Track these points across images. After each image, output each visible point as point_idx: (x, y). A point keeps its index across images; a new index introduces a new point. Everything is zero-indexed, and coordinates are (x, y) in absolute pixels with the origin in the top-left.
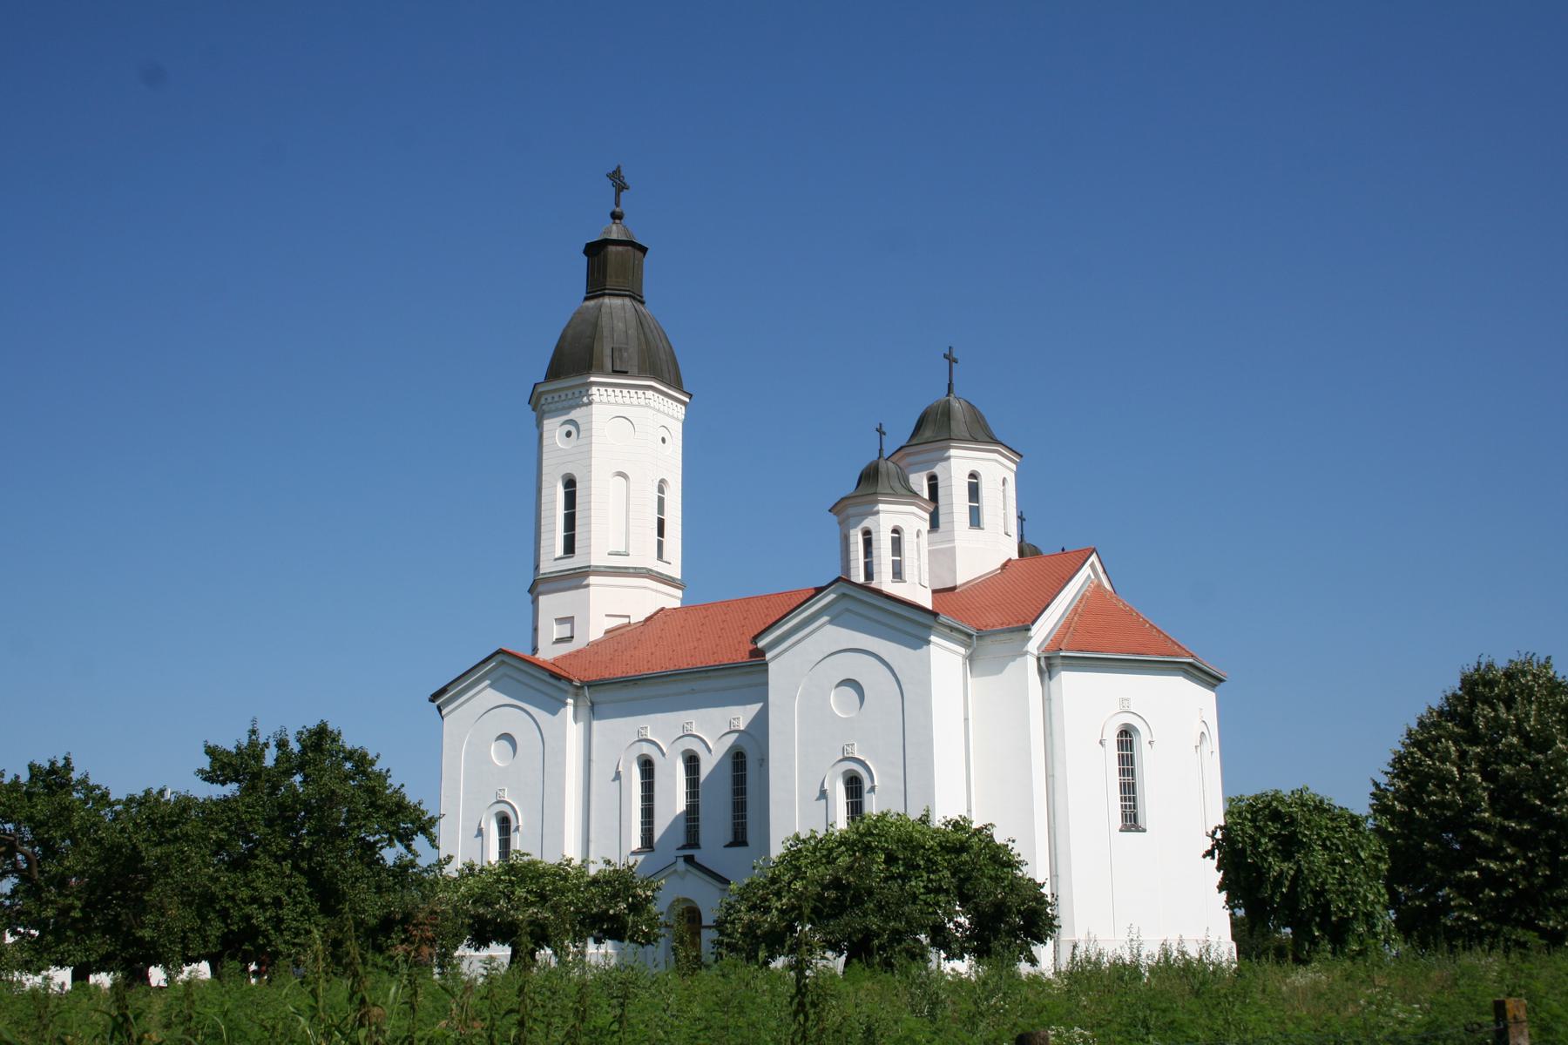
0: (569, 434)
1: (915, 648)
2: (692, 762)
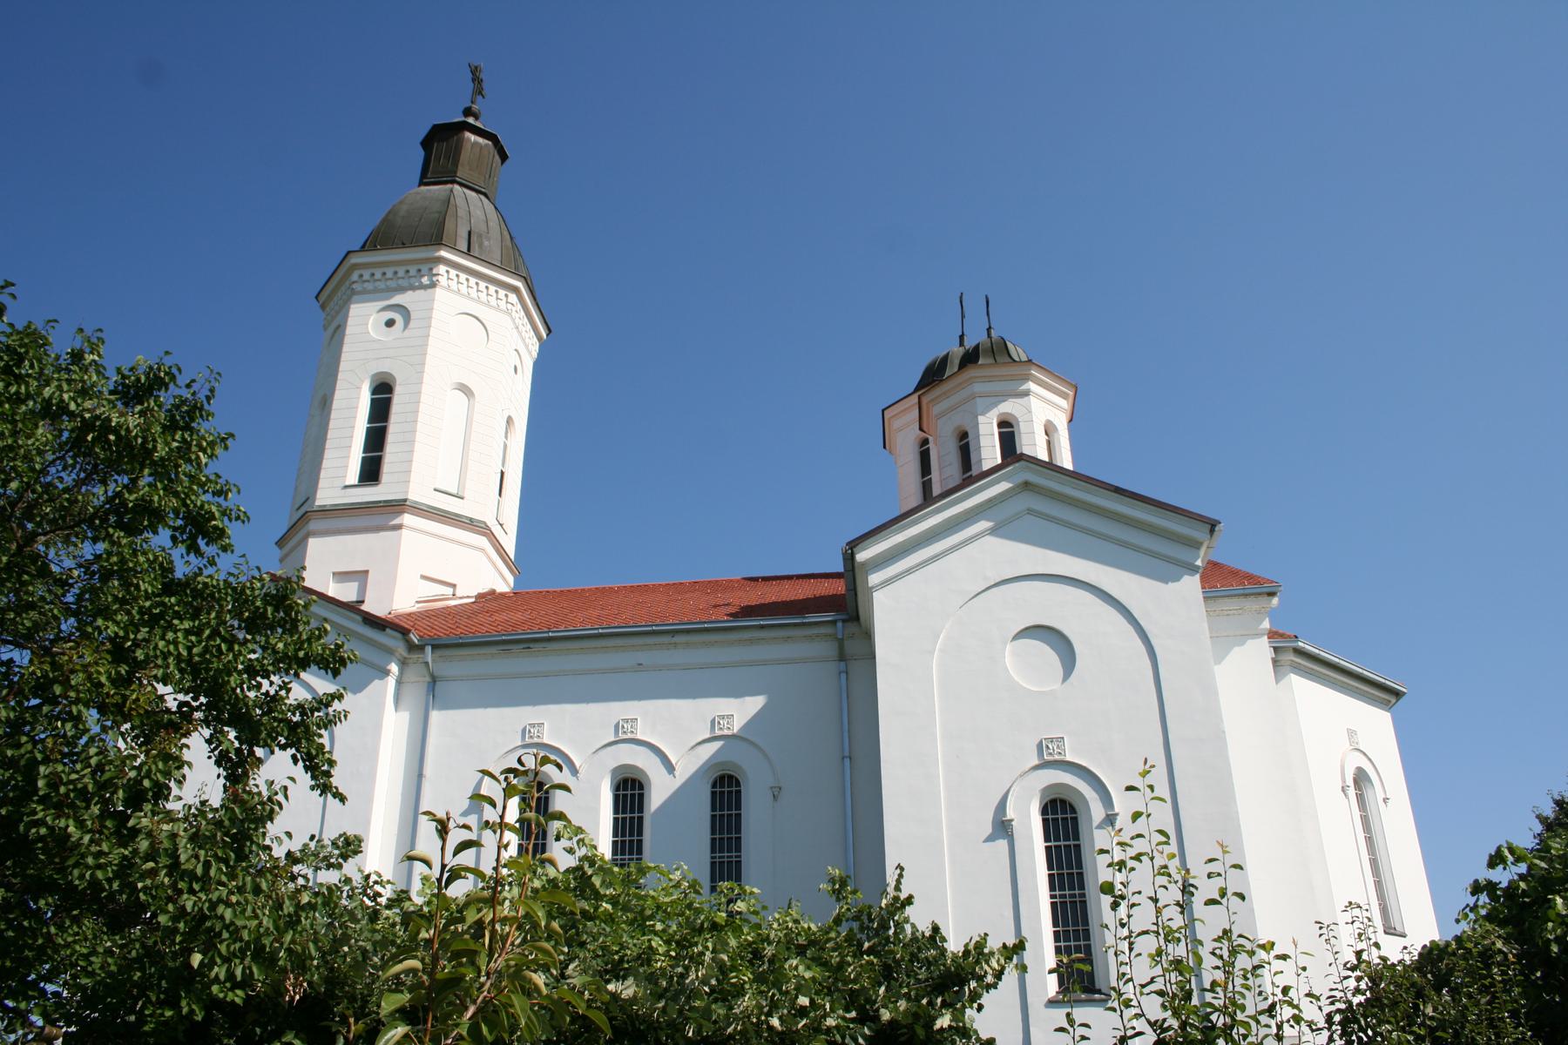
0: (390, 323)
1: (1165, 579)
2: (630, 791)
